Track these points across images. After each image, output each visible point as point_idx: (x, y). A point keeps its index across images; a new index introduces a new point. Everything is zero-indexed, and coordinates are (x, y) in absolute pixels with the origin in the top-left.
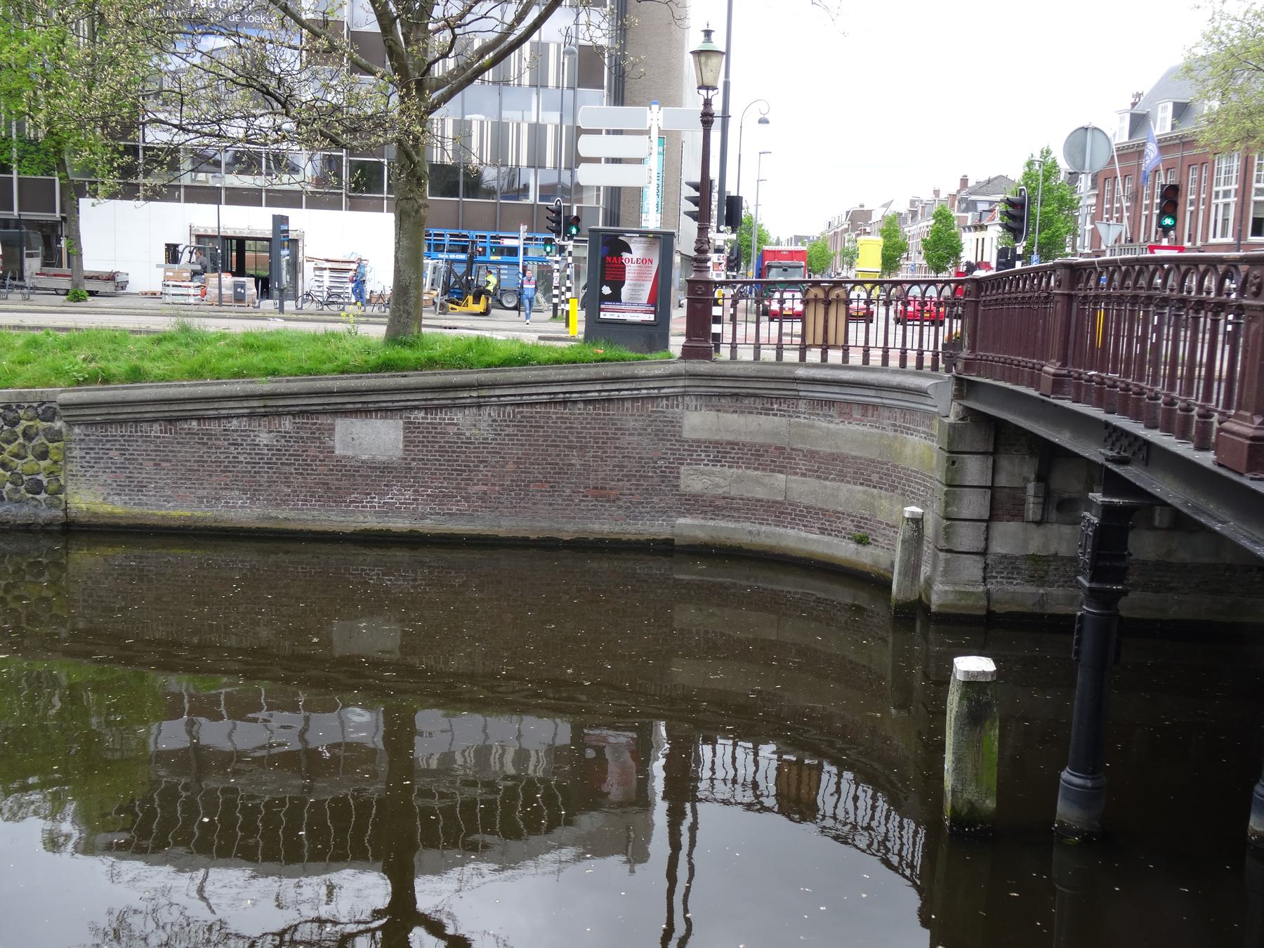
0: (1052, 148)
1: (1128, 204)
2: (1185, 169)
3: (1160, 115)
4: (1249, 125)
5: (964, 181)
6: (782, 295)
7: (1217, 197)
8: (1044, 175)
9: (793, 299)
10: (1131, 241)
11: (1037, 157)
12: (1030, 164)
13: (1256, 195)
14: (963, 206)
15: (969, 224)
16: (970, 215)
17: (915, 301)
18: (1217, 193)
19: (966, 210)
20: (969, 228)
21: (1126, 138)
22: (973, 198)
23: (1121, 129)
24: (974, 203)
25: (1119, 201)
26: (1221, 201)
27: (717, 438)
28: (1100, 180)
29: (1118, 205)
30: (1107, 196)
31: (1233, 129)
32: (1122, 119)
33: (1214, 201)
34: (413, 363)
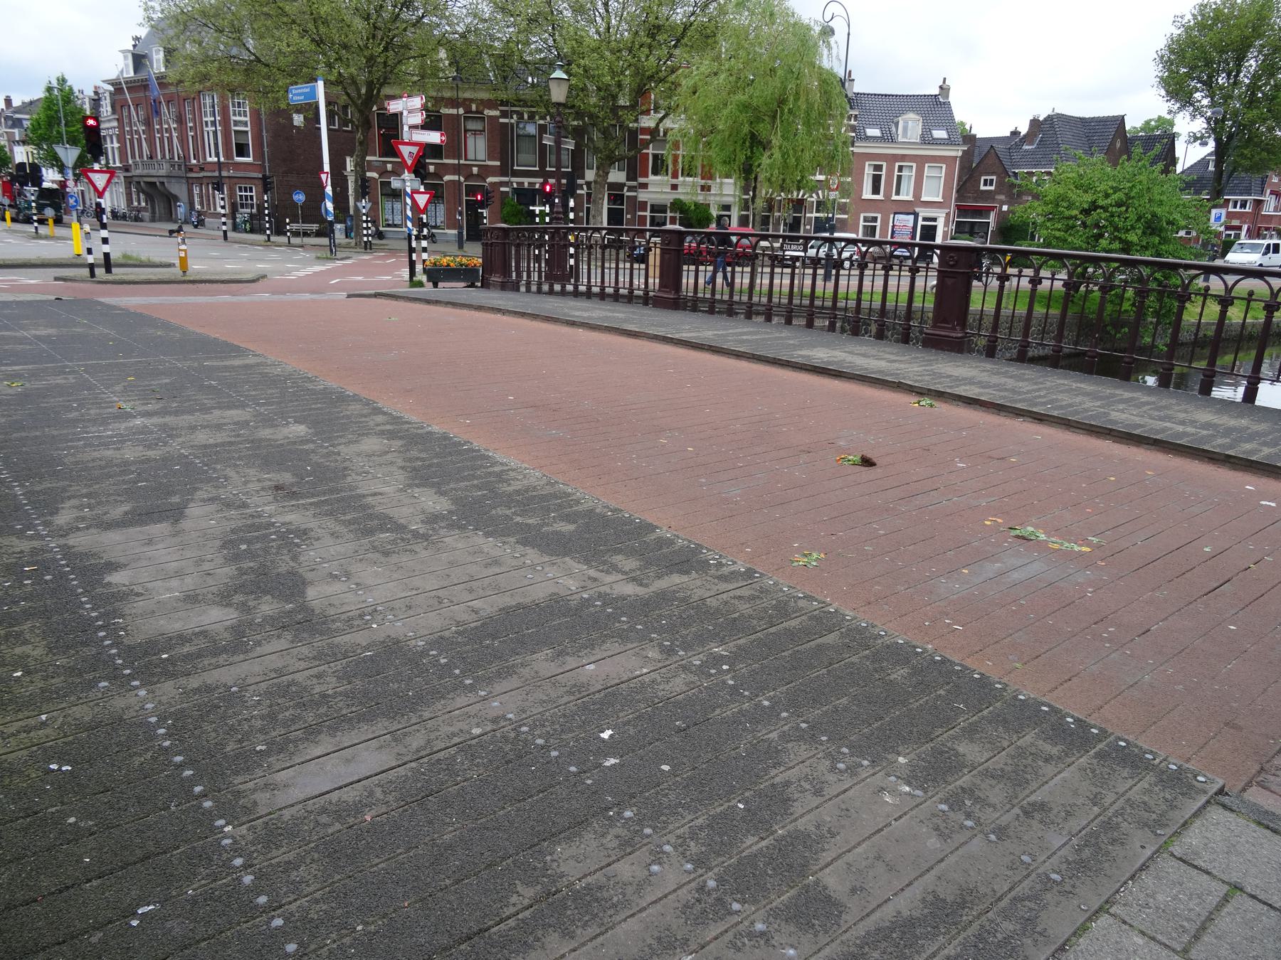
0: (66, 77)
1: (175, 126)
2: (182, 102)
3: (155, 57)
4: (202, 68)
5: (8, 101)
6: (1004, 270)
7: (207, 126)
8: (63, 100)
9: (1019, 276)
10: (151, 158)
11: (55, 84)
12: (49, 89)
13: (235, 125)
14: (10, 123)
15: (17, 139)
16: (16, 131)
17: (596, 245)
18: (206, 122)
19: (13, 126)
20: (18, 142)
21: (132, 74)
22: (18, 116)
23: (127, 65)
24: (20, 120)
25: (136, 125)
26: (211, 129)
27: (984, 666)
28: (118, 108)
29: (166, 126)
30: (126, 121)
31: (191, 72)
32: (126, 58)
33: (205, 129)
34: (528, 500)
